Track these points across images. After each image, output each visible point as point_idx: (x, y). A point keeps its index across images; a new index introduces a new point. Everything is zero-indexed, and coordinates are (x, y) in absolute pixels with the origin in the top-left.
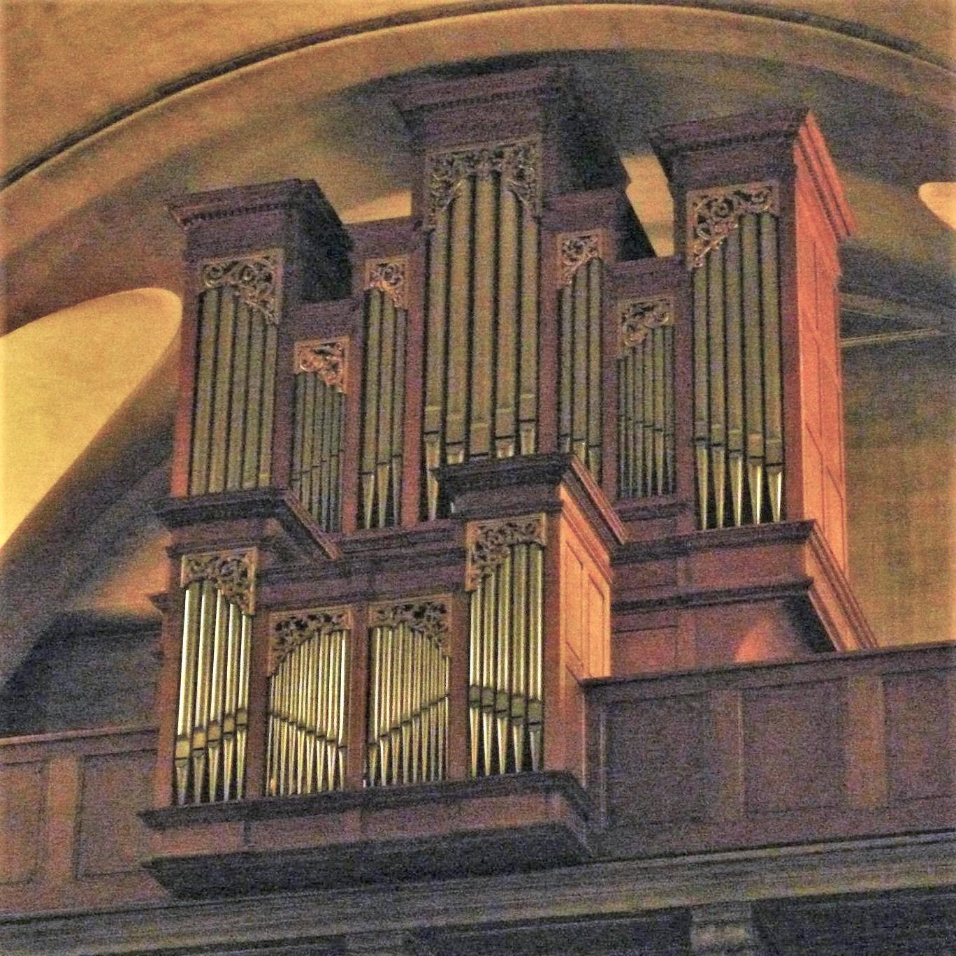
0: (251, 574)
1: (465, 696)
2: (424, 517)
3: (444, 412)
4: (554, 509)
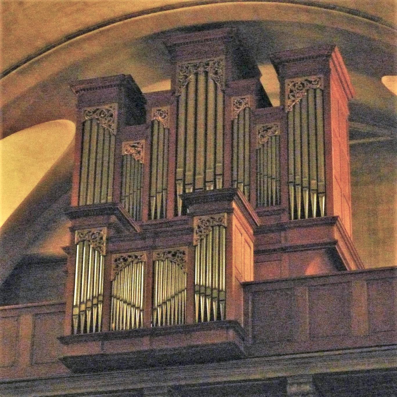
0: (104, 238)
1: (193, 289)
2: (176, 215)
3: (185, 171)
4: (230, 211)
